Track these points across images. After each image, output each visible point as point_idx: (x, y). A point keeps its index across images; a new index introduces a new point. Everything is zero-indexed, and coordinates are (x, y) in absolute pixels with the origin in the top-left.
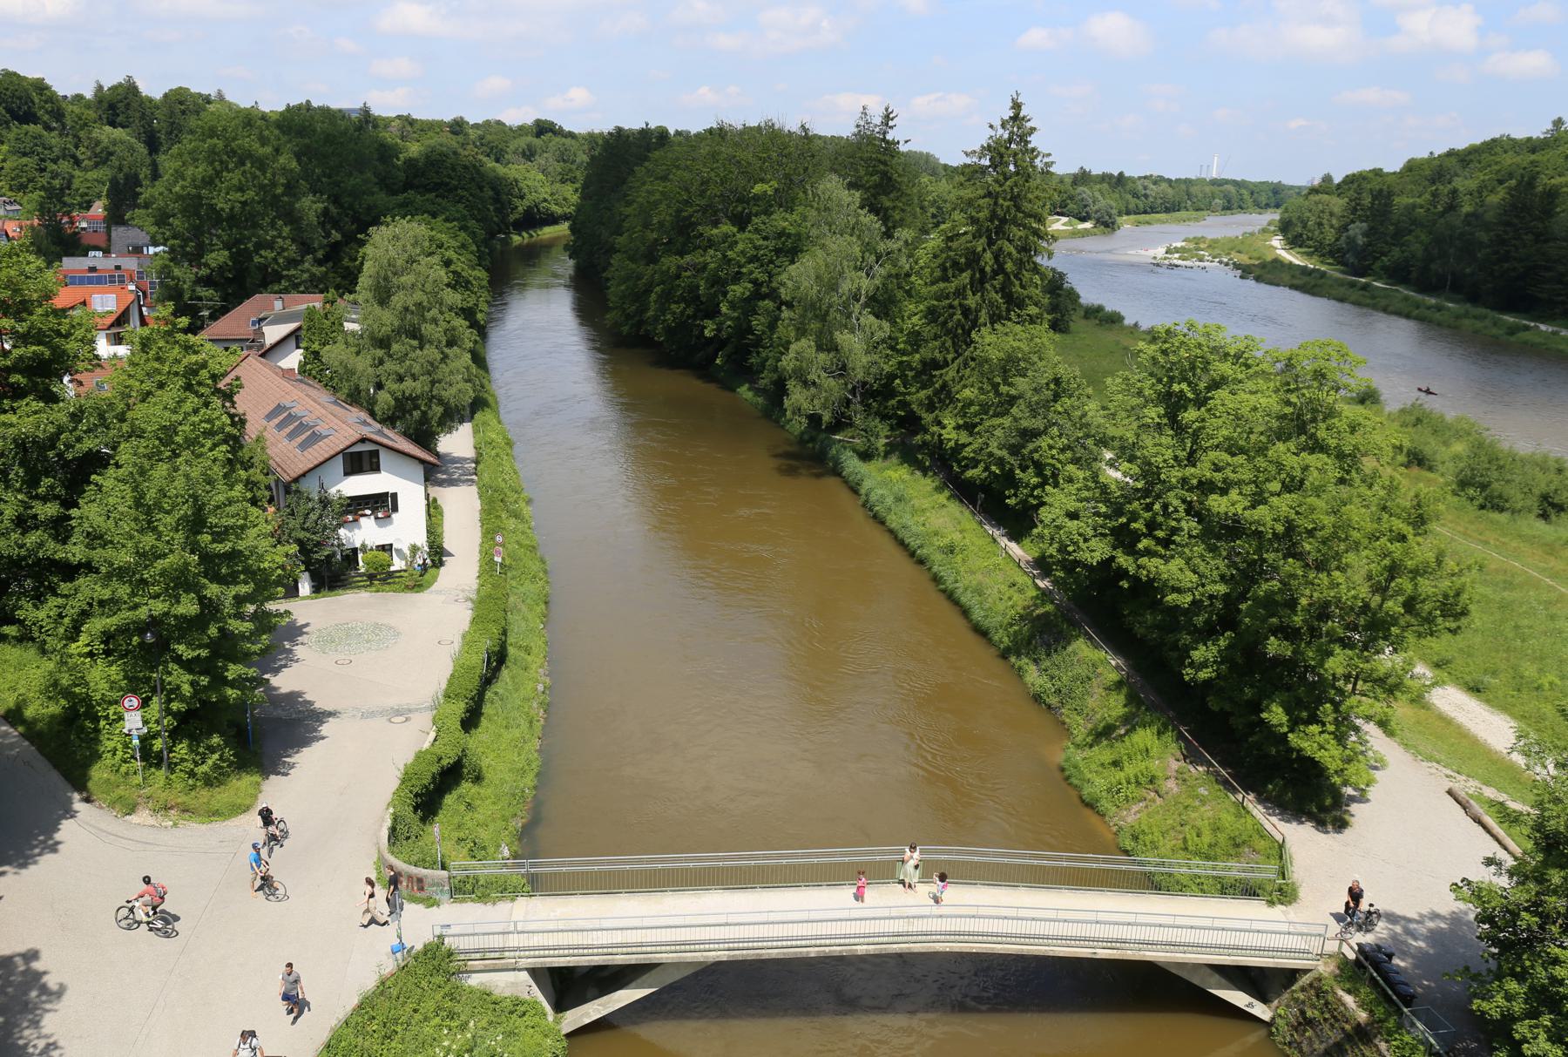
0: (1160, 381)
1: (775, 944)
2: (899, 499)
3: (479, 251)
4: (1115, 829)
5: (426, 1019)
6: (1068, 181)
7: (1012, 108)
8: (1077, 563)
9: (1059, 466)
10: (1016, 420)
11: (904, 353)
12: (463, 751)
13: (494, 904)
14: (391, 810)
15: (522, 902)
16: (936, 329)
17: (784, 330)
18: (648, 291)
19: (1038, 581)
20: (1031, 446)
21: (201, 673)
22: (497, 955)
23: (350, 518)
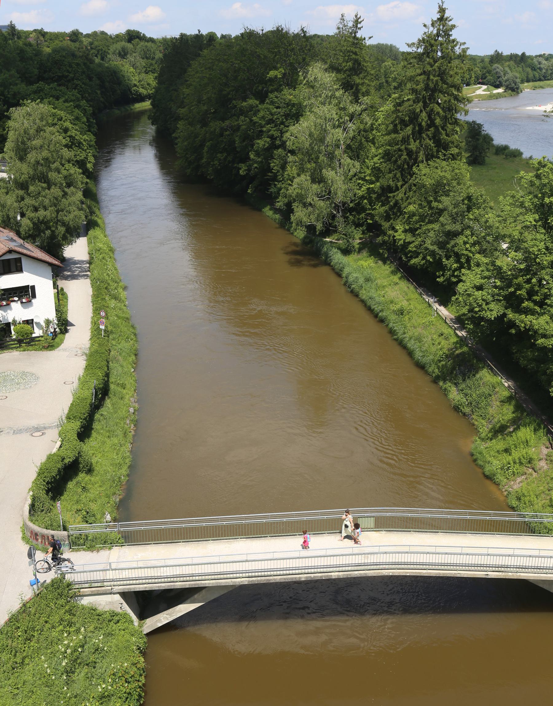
0: (536, 196)
1: (278, 573)
2: (368, 280)
3: (88, 121)
4: (505, 493)
5: (53, 627)
6: (487, 60)
7: (439, 12)
8: (482, 319)
9: (471, 255)
10: (443, 225)
11: (372, 182)
12: (79, 453)
13: (98, 551)
14: (31, 493)
15: (116, 550)
16: (389, 166)
17: (291, 170)
18: (202, 145)
19: (457, 332)
20: (452, 243)
22: (99, 584)
23: (4, 303)
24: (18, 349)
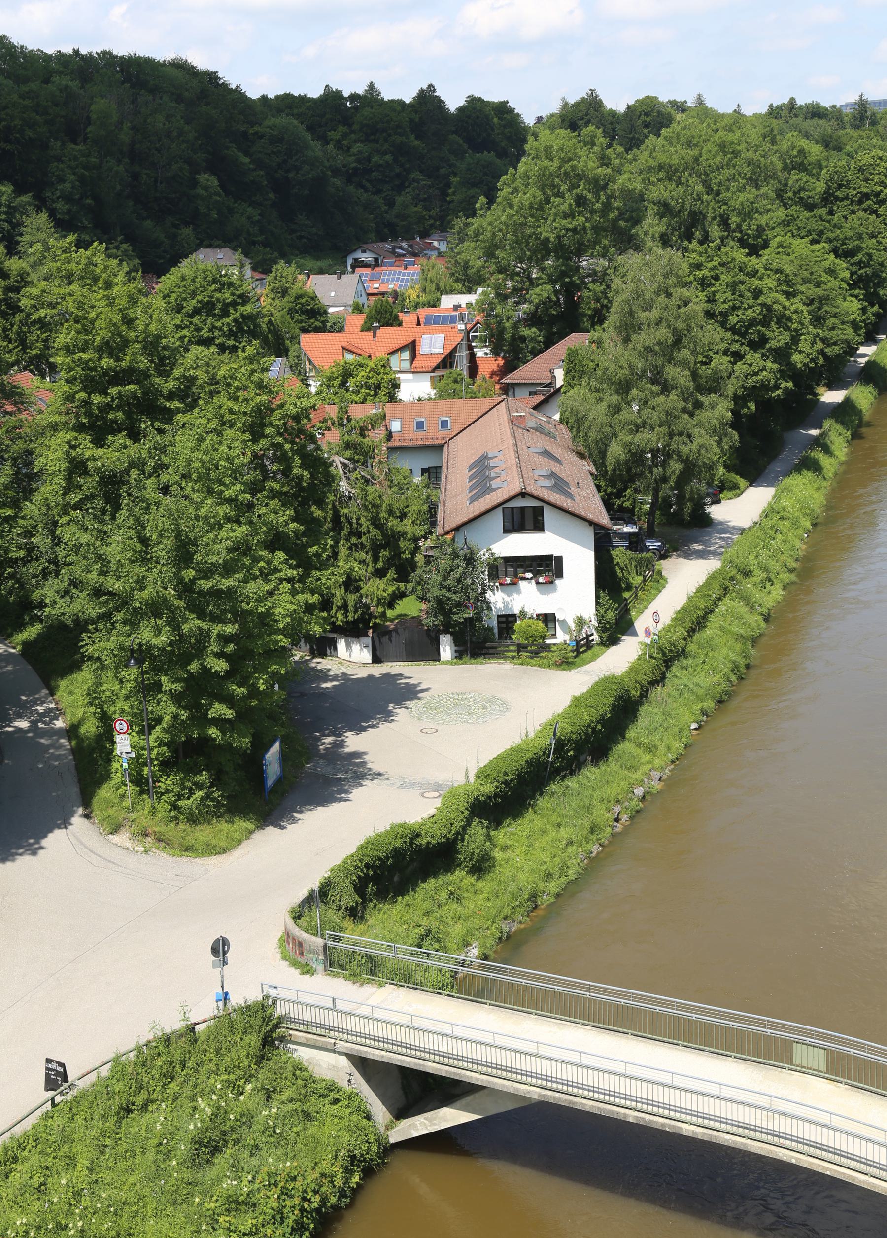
13: (362, 984)
21: (184, 708)
24: (515, 661)
